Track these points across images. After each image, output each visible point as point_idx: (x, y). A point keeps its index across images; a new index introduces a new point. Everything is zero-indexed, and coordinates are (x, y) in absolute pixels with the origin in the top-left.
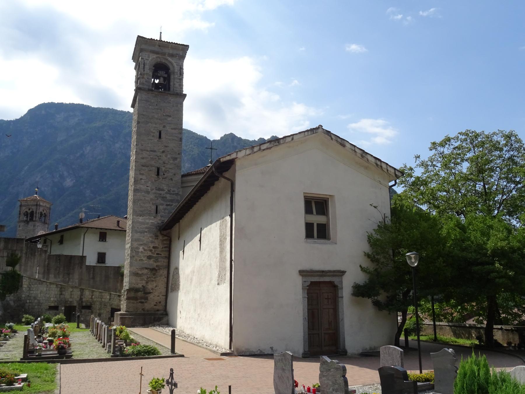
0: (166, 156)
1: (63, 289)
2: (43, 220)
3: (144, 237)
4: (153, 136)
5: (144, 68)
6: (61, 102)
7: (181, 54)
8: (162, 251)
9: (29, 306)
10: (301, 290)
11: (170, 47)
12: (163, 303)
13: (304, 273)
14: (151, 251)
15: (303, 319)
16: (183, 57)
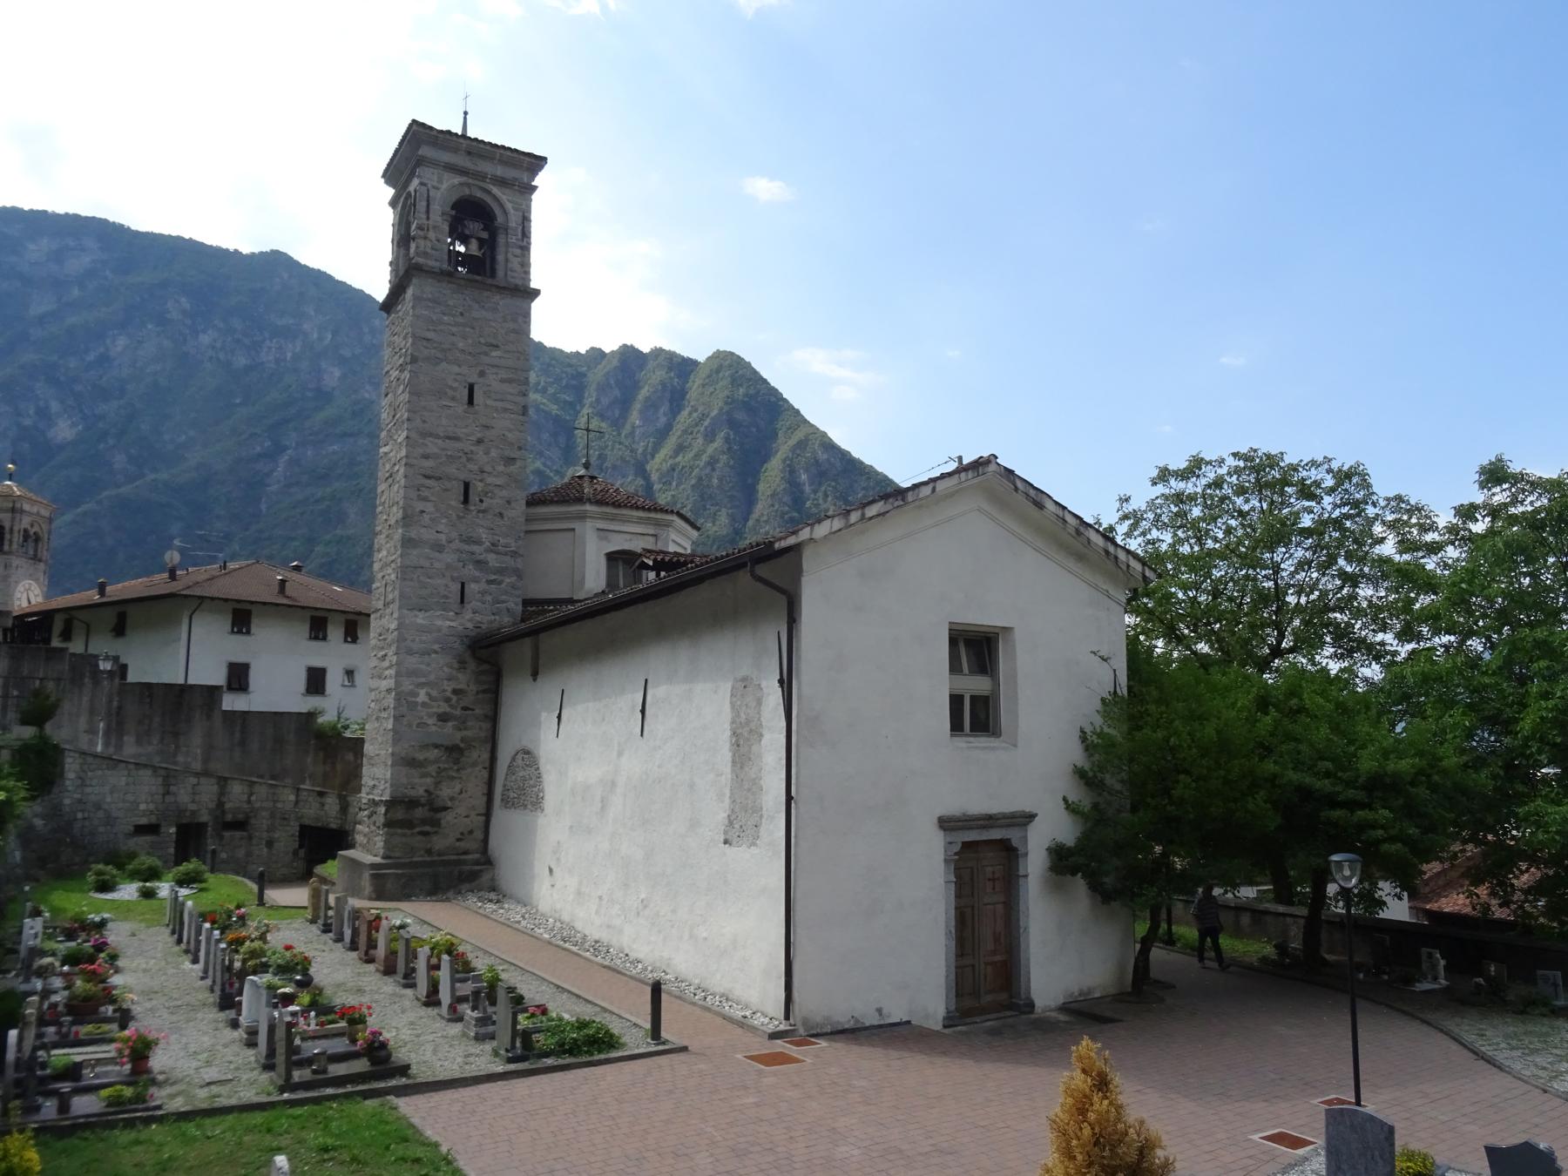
2: (31, 552)
3: (428, 665)
4: (453, 399)
5: (428, 212)
9: (83, 827)
10: (943, 865)
12: (479, 835)
14: (448, 700)
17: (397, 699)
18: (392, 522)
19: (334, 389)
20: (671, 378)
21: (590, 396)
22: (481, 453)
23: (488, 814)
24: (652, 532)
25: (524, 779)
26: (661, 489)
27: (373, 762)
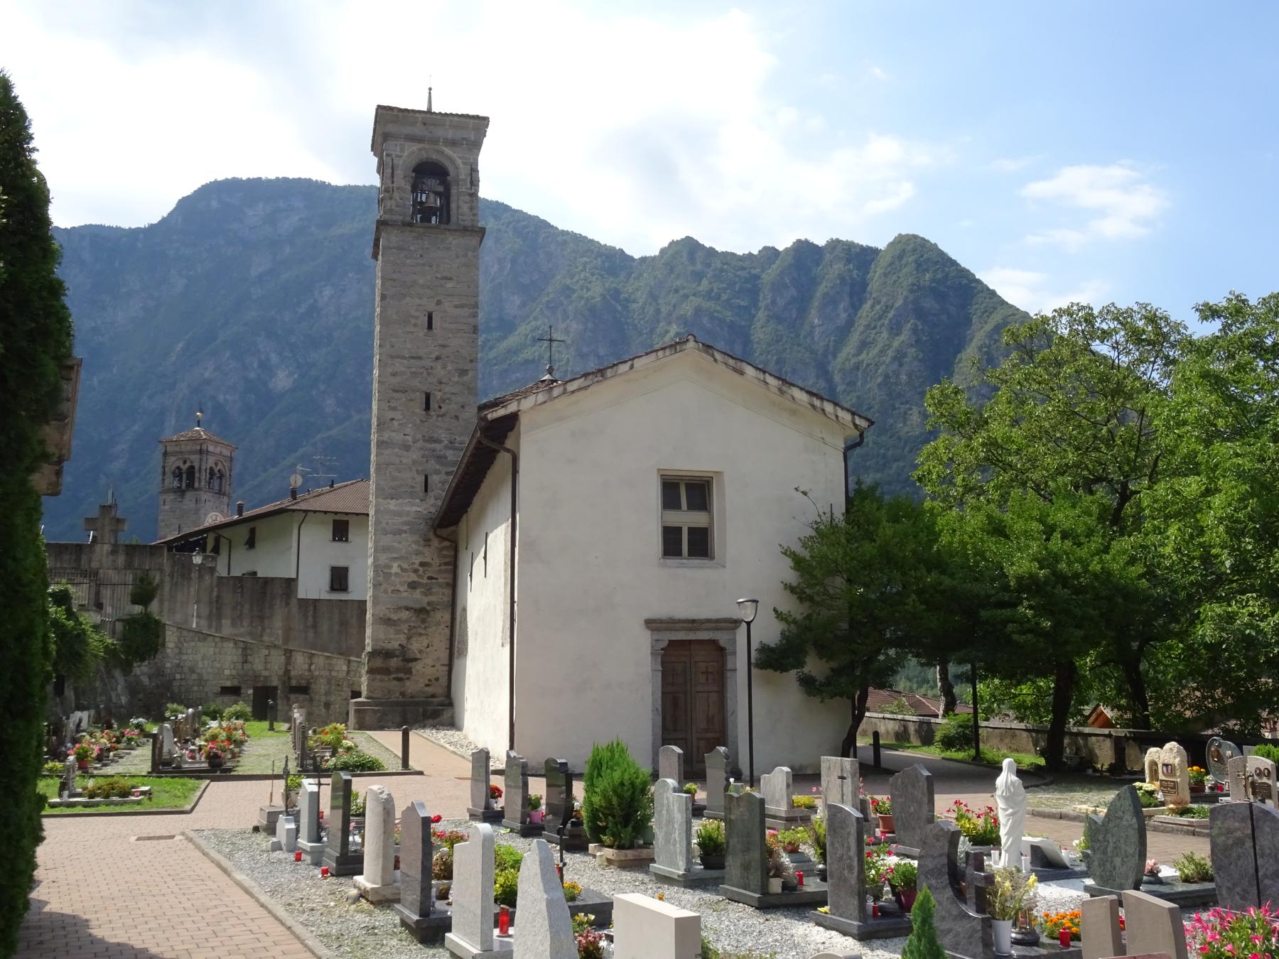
0: (444, 367)
1: (249, 652)
3: (400, 542)
4: (415, 325)
6: (255, 177)
7: (473, 138)
8: (440, 572)
11: (448, 123)
12: (444, 681)
13: (654, 625)
14: (416, 571)
15: (653, 711)
16: (476, 145)
20: (849, 270)
21: (765, 298)
26: (845, 390)
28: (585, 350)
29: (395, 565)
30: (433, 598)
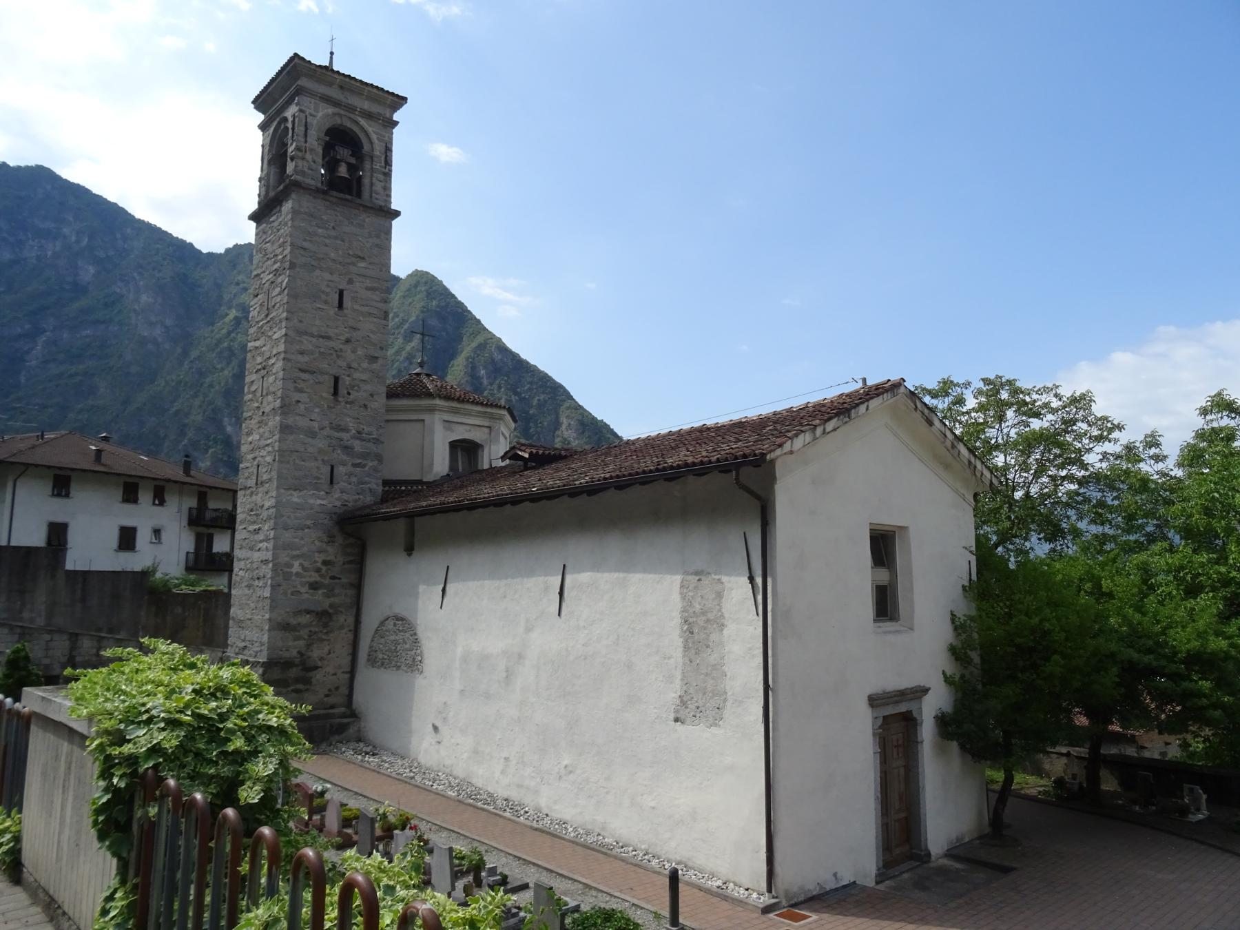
3: (302, 539)
4: (326, 302)
5: (306, 135)
14: (318, 570)
17: (274, 570)
18: (267, 409)
19: (89, 283)
22: (349, 351)
23: (352, 672)
24: (487, 424)
25: (396, 643)
27: (243, 625)
28: (153, 319)
29: (296, 564)
30: (336, 600)
